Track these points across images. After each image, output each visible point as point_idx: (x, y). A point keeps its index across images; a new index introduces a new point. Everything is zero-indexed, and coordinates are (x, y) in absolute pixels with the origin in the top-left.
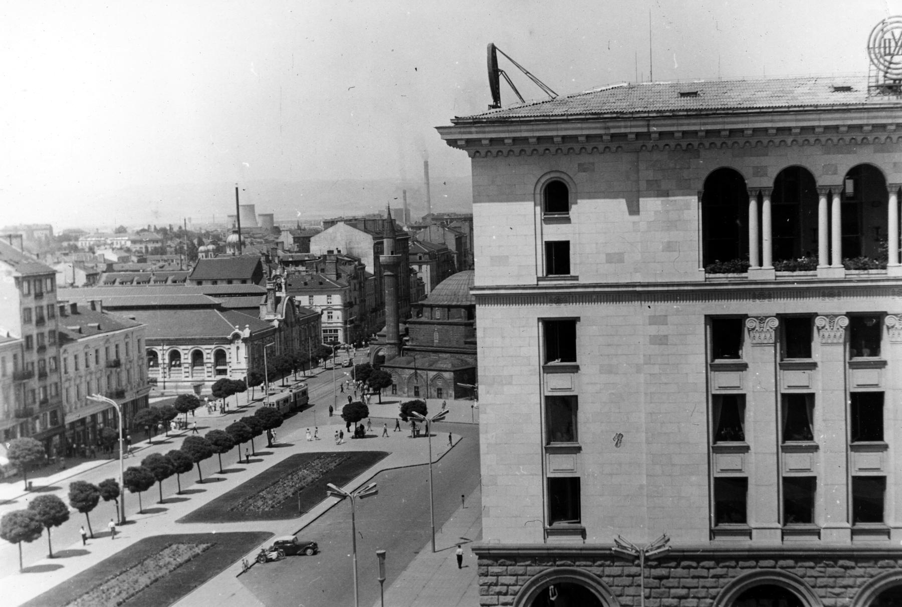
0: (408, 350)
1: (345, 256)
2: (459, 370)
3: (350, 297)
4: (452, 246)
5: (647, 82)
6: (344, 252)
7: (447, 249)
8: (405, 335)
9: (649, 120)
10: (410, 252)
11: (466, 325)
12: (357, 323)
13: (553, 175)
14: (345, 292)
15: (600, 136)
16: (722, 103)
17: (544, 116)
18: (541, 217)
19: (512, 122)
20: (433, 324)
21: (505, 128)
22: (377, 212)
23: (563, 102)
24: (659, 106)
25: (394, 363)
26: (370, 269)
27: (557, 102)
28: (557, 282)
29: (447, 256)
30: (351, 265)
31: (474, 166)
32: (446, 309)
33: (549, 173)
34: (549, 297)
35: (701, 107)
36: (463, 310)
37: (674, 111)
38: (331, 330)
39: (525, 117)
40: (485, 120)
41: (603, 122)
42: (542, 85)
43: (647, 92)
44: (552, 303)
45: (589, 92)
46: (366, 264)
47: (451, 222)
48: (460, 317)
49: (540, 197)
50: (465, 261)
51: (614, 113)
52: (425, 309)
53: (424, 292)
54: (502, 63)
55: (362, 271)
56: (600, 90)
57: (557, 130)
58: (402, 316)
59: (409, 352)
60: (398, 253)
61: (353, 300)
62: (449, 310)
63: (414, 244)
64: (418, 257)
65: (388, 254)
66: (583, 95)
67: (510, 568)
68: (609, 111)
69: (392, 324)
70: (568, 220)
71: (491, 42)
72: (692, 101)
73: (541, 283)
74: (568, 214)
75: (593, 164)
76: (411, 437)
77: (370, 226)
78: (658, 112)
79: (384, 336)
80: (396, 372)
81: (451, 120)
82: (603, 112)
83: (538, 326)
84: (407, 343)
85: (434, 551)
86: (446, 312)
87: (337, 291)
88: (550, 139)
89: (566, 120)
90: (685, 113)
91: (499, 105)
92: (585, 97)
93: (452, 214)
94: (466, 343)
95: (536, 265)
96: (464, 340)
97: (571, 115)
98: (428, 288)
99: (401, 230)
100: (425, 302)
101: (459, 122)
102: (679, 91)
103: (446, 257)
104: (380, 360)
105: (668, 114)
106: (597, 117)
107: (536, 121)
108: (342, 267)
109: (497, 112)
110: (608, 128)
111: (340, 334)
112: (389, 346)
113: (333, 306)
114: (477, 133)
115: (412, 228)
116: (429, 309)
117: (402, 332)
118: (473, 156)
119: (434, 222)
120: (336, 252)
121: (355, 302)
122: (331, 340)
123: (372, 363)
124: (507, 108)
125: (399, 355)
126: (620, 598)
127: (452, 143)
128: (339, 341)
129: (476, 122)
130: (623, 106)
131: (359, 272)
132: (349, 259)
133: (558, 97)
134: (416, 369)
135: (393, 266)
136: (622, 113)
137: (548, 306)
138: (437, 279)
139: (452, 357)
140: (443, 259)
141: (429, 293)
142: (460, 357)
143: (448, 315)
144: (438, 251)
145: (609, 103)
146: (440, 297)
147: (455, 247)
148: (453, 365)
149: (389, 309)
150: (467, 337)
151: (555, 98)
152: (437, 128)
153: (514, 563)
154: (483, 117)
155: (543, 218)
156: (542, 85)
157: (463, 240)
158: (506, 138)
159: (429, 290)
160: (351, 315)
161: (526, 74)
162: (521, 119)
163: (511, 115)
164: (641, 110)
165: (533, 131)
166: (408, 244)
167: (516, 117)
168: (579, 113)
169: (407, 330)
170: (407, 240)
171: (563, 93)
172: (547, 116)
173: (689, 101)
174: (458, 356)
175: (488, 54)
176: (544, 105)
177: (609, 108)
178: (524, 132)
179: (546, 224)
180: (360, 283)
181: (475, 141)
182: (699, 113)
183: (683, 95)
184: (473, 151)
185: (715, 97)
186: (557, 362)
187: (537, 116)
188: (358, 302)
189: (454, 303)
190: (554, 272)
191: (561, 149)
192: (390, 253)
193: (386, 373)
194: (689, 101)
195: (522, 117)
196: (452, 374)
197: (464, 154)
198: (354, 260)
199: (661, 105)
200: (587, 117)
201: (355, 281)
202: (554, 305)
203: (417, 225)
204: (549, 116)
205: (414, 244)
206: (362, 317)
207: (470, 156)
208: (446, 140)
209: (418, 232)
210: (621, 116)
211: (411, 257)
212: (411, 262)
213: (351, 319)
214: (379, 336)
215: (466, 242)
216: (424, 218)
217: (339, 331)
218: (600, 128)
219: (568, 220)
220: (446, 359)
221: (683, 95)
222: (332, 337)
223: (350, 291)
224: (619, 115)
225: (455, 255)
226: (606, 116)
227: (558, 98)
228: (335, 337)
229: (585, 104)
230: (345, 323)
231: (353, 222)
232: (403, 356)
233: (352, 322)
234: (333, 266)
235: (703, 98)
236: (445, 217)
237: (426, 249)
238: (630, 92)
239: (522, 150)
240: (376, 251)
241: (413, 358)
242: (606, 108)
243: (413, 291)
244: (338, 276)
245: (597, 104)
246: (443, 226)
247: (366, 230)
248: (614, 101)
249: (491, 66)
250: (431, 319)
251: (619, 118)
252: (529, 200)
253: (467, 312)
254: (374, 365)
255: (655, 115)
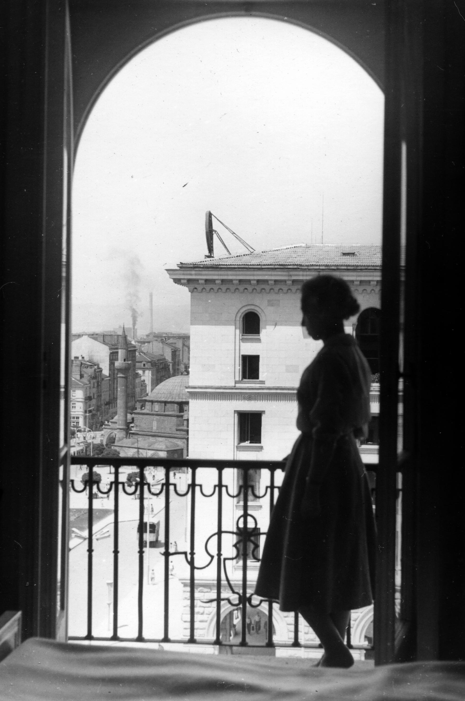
0: (133, 434)
1: (88, 361)
2: (171, 450)
3: (90, 393)
4: (169, 357)
5: (319, 243)
6: (87, 358)
7: (165, 359)
8: (131, 423)
9: (320, 271)
10: (137, 360)
11: (178, 416)
12: (94, 412)
13: (249, 307)
14: (86, 389)
15: (285, 281)
16: (373, 262)
17: (244, 265)
18: (240, 337)
19: (221, 268)
20: (153, 415)
21: (216, 273)
22: (112, 330)
23: (258, 256)
24: (326, 262)
25: (122, 444)
26: (106, 372)
27: (254, 256)
28: (250, 384)
29: (165, 364)
30: (91, 368)
31: (192, 298)
32: (163, 404)
33: (247, 305)
34: (243, 396)
35: (357, 264)
36: (176, 405)
37: (338, 266)
38: (74, 417)
39: (231, 265)
40: (202, 266)
41: (287, 271)
42: (243, 242)
43: (319, 251)
44: (245, 400)
45: (277, 249)
46: (103, 368)
47: (169, 339)
48: (173, 410)
49: (239, 323)
50: (178, 369)
51: (295, 265)
52: (147, 403)
53: (146, 391)
54: (216, 225)
55: (99, 373)
56: (285, 248)
57: (254, 275)
58: (129, 409)
59: (133, 435)
60: (129, 361)
61: (92, 395)
62: (165, 405)
63: (140, 354)
64: (142, 365)
65: (122, 361)
66: (273, 251)
67: (206, 594)
68: (292, 264)
69: (122, 414)
70: (259, 340)
71: (209, 210)
72: (351, 259)
73: (238, 385)
74: (259, 336)
75: (279, 301)
76: (133, 499)
77: (108, 339)
78: (326, 266)
79: (116, 423)
80: (123, 450)
81: (177, 265)
82: (287, 264)
83: (234, 417)
84: (132, 429)
85: (149, 584)
86: (163, 407)
87: (79, 387)
88: (249, 281)
89: (260, 268)
90: (346, 268)
91: (212, 255)
92: (274, 252)
93: (169, 333)
94: (177, 430)
95: (235, 372)
96: (176, 428)
97: (264, 265)
98: (149, 388)
99: (131, 344)
100: (147, 398)
101: (183, 267)
102: (342, 251)
103: (164, 366)
104: (112, 440)
105: (333, 268)
106: (283, 268)
107: (239, 268)
108: (85, 370)
109: (211, 260)
110: (291, 276)
111: (81, 421)
112: (119, 430)
113: (77, 399)
114: (196, 275)
115: (139, 342)
116: (150, 403)
117: (130, 420)
118: (192, 291)
119: (156, 339)
120: (80, 358)
121: (94, 396)
122: (74, 425)
123: (104, 443)
124: (218, 258)
125: (126, 437)
126: (286, 619)
127: (177, 281)
128: (80, 425)
129: (195, 267)
130: (302, 260)
131: (98, 374)
132: (91, 364)
133: (255, 252)
134: (138, 448)
135: (125, 370)
136: (301, 265)
137: (243, 401)
138: (157, 381)
139: (166, 440)
140: (161, 367)
141: (150, 392)
142: (172, 441)
143: (165, 409)
144: (158, 360)
145: (292, 258)
146: (160, 395)
147: (171, 358)
148: (167, 447)
149: (120, 402)
150: (178, 425)
151: (252, 252)
152: (166, 270)
153: (209, 590)
154: (201, 263)
155: (241, 338)
156: (243, 242)
157: (177, 353)
158: (217, 280)
159: (150, 390)
160: (90, 407)
161: (232, 234)
162: (228, 266)
163: (221, 263)
164: (314, 264)
165: (236, 275)
166: (135, 354)
167: (224, 265)
168: (270, 264)
169: (133, 419)
170: (135, 351)
171: (258, 250)
172: (247, 265)
173: (348, 259)
174: (170, 440)
175: (206, 218)
176: (244, 257)
177: (292, 261)
178: (230, 276)
179: (243, 342)
180: (98, 382)
181: (194, 281)
182: (355, 268)
183: (344, 254)
184: (192, 288)
185: (367, 257)
186: (247, 443)
187: (240, 265)
188: (96, 397)
189: (169, 400)
190: (247, 378)
191: (256, 289)
192: (123, 360)
193: (116, 451)
194: (348, 259)
195: (229, 265)
196: (166, 453)
197: (185, 290)
198: (93, 364)
199: (329, 261)
200: (276, 267)
201: (95, 381)
202: (246, 401)
203: (142, 340)
204: (248, 265)
205: (140, 354)
206: (98, 408)
207: (190, 291)
208: (173, 279)
209: (143, 345)
210: (300, 268)
211: (137, 364)
212: (137, 368)
213: (90, 409)
214: (111, 422)
215: (179, 355)
216: (148, 336)
217: (80, 418)
218: (285, 275)
219: (259, 340)
220: (162, 442)
221: (344, 254)
222: (74, 422)
223: (90, 388)
224: (298, 267)
225: (171, 364)
226: (289, 267)
227: (255, 252)
228: (77, 423)
229: (274, 258)
230: (85, 412)
231: (94, 336)
232: (129, 438)
233: (90, 411)
234: (78, 369)
235: (359, 257)
236: (164, 335)
237: (150, 359)
238: (307, 250)
239: (228, 289)
240: (111, 358)
241: (136, 440)
242: (290, 261)
243: (138, 390)
244: (82, 376)
245: (283, 258)
246: (162, 342)
247: (104, 343)
248: (295, 256)
249: (208, 227)
250: (152, 411)
251: (299, 269)
252: (231, 325)
253: (179, 407)
254: (107, 445)
255: (324, 268)
